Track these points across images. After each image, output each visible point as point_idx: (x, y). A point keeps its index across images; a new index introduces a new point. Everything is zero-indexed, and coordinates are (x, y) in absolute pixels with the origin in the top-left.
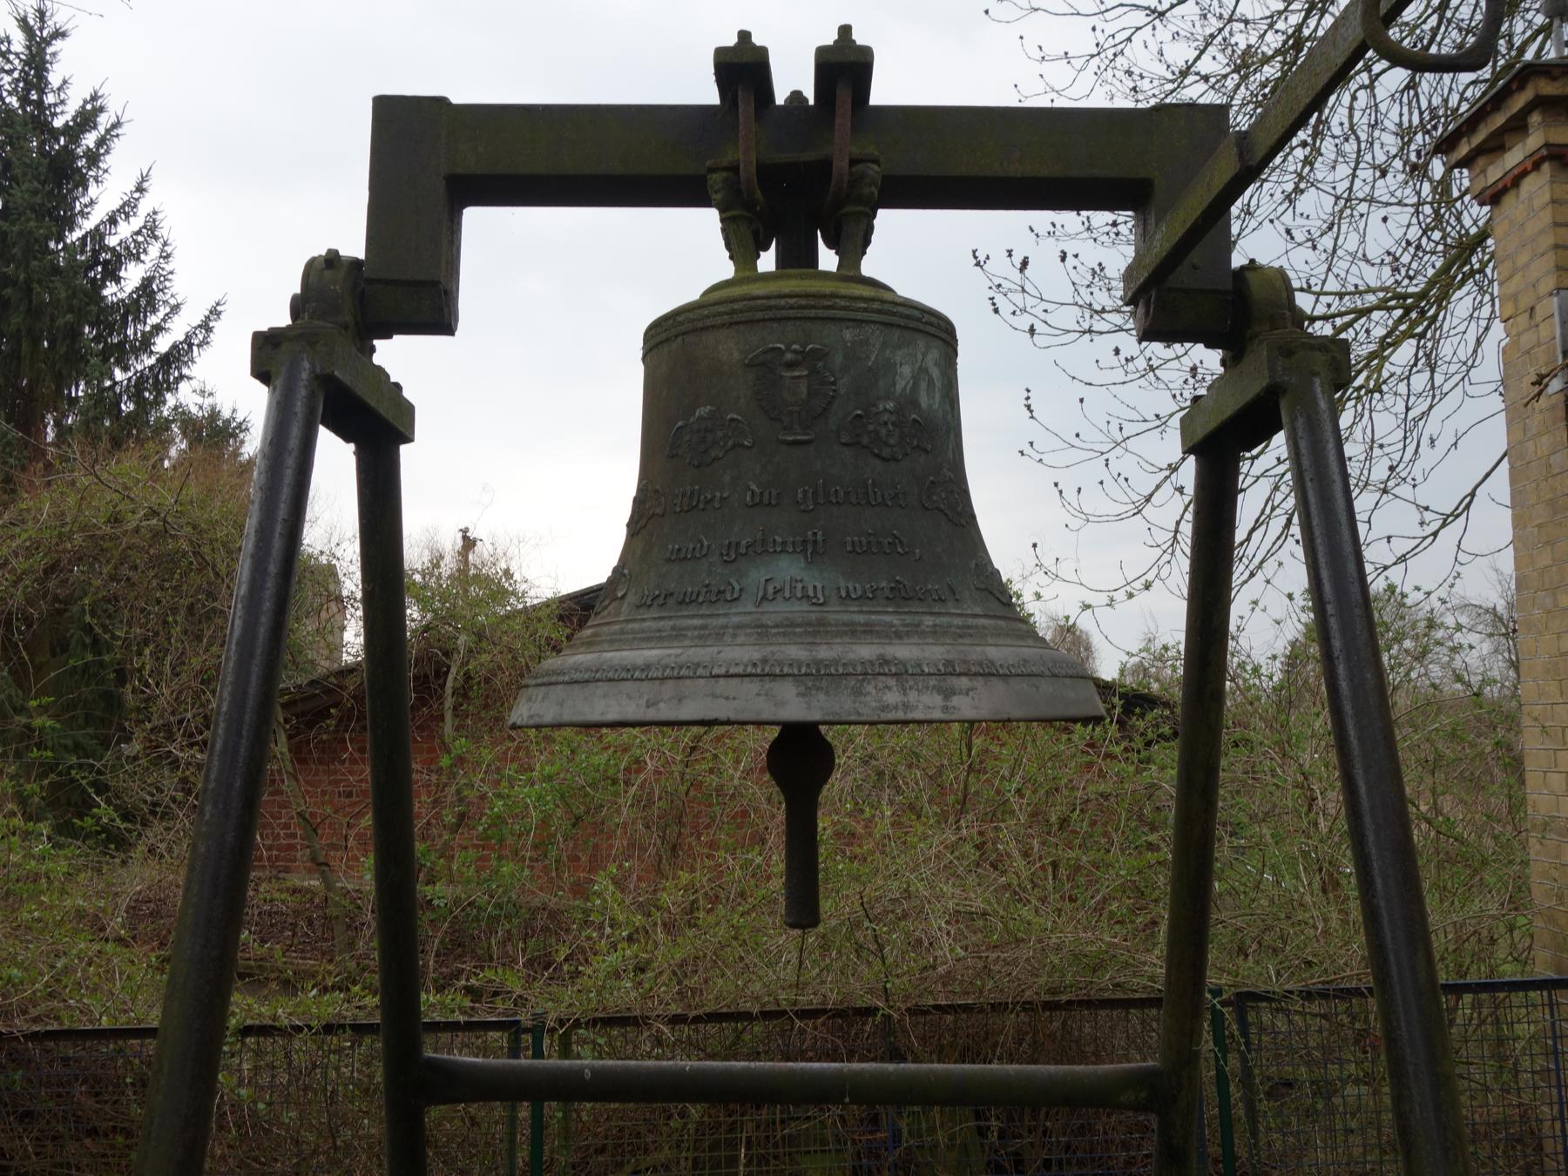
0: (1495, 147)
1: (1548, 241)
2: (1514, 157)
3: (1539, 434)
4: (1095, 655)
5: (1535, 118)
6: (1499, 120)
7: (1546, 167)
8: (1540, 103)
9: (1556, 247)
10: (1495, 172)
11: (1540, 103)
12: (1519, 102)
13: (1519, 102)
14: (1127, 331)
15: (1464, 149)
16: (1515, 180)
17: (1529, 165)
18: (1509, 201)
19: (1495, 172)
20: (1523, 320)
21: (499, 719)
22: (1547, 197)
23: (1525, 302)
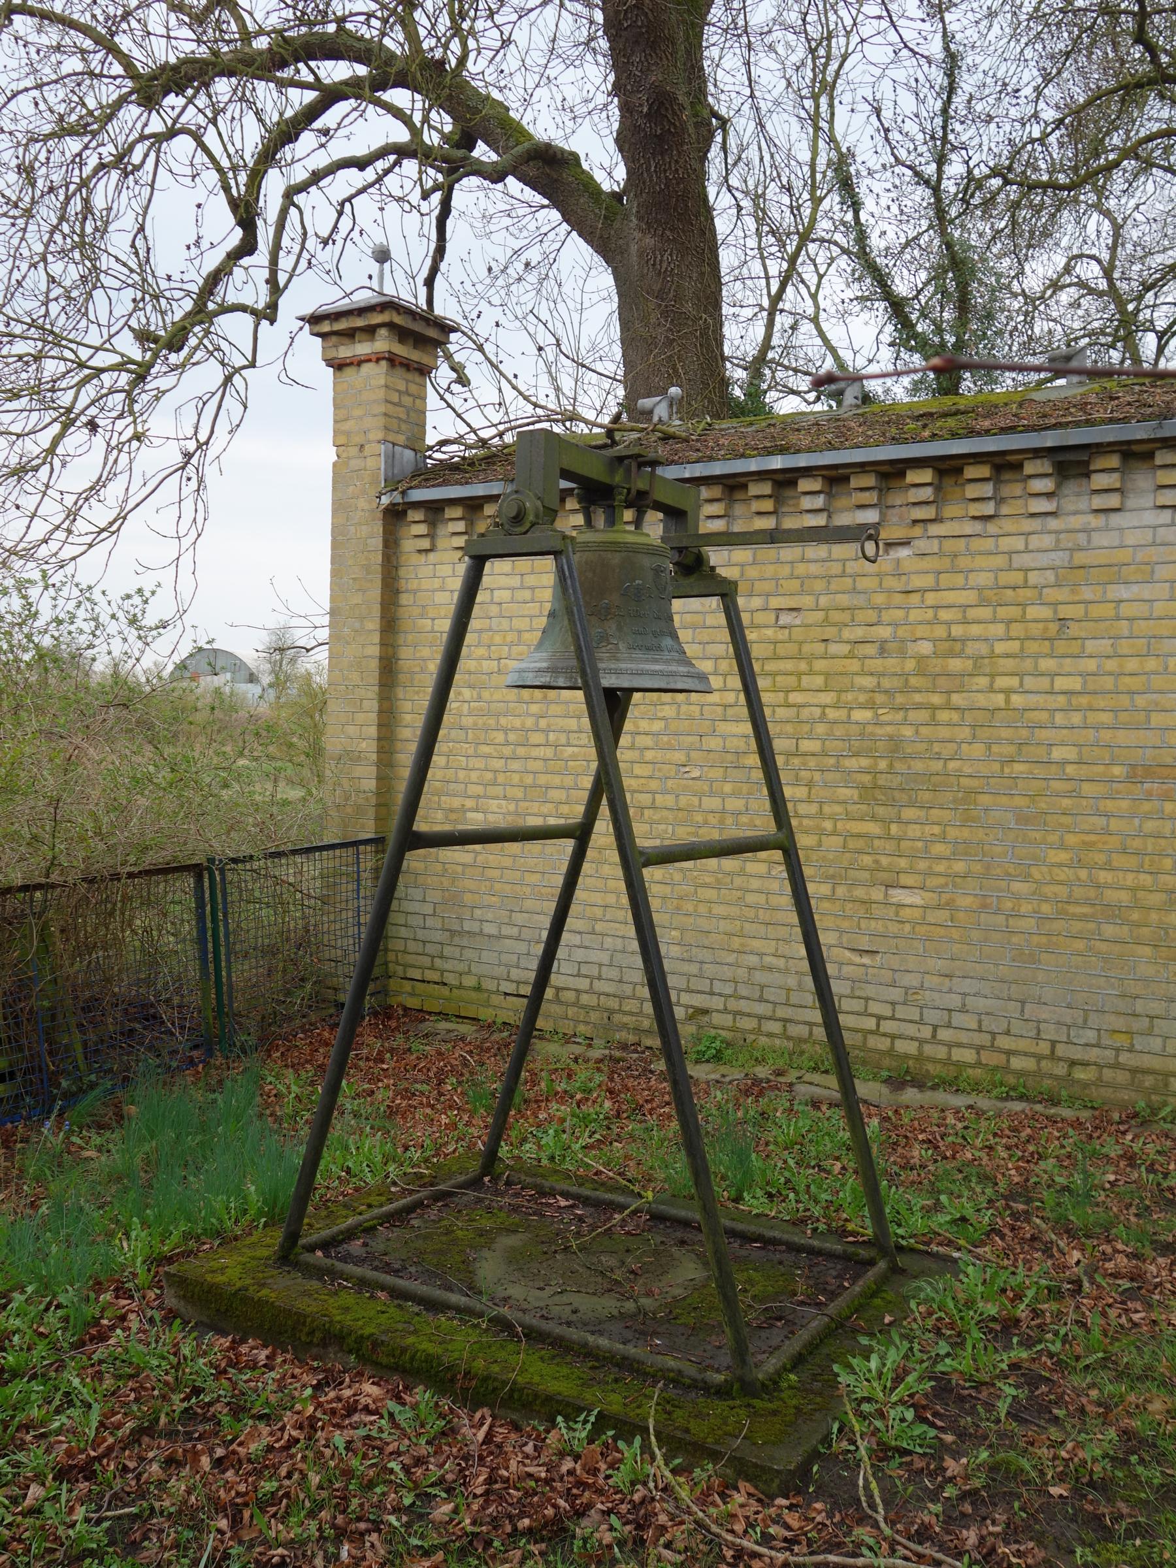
0: (350, 335)
1: (382, 409)
2: (362, 348)
3: (360, 524)
4: (402, 677)
5: (383, 332)
6: (359, 322)
7: (384, 363)
8: (390, 325)
9: (385, 414)
10: (345, 352)
11: (390, 325)
12: (377, 319)
13: (377, 319)
14: (130, 315)
15: (326, 327)
16: (359, 363)
17: (374, 357)
18: (349, 372)
19: (345, 352)
20: (354, 451)
21: (604, 614)
22: (382, 382)
23: (358, 439)
